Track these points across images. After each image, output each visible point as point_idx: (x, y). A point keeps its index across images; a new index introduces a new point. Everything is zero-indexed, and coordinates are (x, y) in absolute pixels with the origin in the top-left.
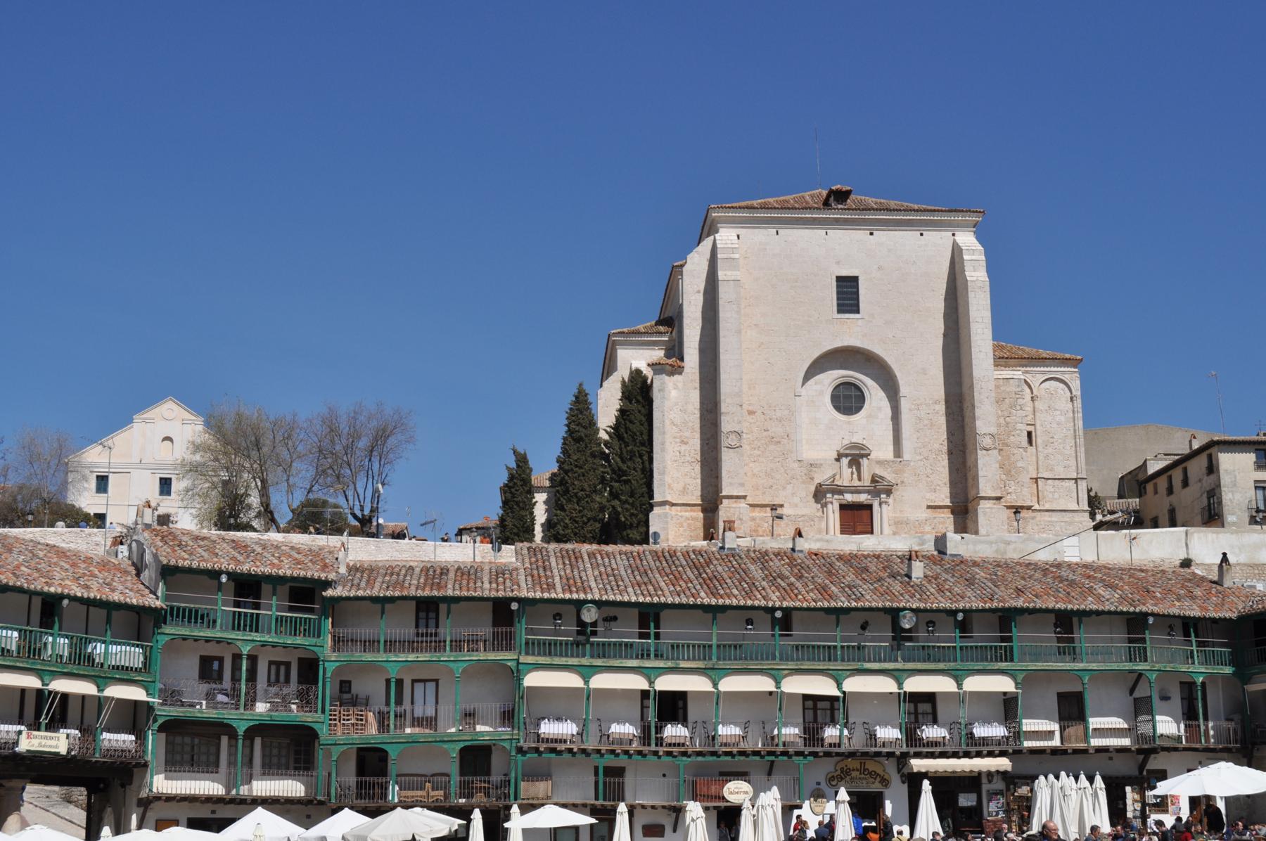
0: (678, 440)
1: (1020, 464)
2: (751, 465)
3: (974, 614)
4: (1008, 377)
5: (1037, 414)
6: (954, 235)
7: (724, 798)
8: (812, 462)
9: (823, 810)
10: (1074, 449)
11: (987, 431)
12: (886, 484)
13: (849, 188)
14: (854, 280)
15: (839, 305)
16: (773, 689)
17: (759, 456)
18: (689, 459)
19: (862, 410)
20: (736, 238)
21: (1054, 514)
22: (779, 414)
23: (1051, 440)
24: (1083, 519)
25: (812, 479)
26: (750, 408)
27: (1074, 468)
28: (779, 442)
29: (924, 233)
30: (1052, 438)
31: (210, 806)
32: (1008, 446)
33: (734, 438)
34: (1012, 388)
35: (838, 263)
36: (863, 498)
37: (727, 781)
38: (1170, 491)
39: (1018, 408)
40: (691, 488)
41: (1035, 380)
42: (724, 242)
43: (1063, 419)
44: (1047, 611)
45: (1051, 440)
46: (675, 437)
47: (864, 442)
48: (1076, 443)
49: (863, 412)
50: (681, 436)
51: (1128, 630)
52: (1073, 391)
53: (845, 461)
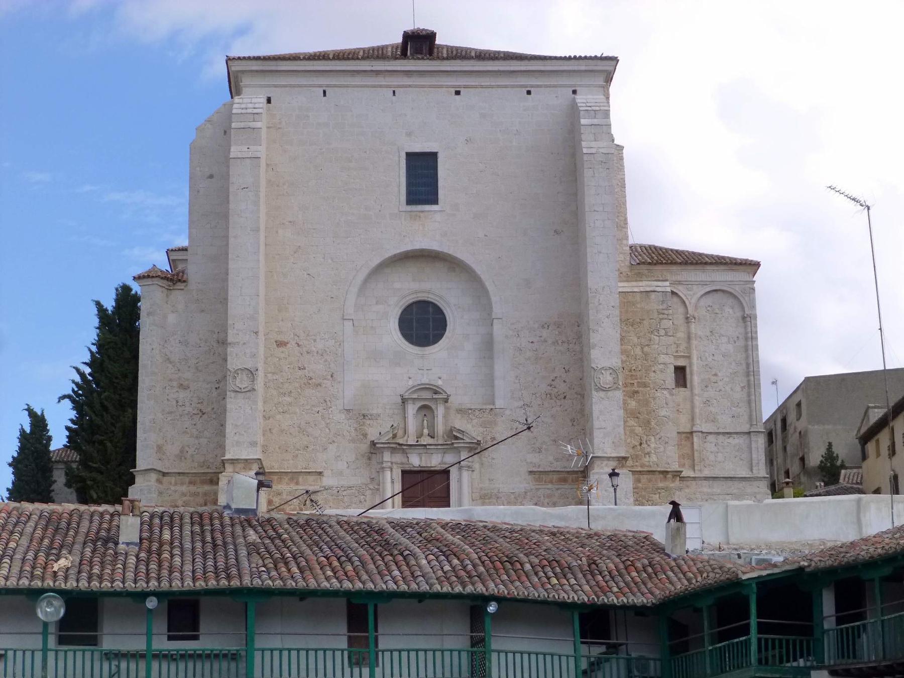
0: (175, 384)
1: (663, 412)
2: (279, 417)
3: (107, 600)
4: (648, 289)
5: (694, 342)
6: (574, 92)
10: (746, 390)
11: (607, 364)
12: (468, 440)
14: (432, 157)
15: (409, 193)
17: (290, 404)
18: (191, 410)
20: (265, 101)
21: (716, 484)
22: (320, 345)
23: (714, 379)
24: (757, 490)
26: (280, 338)
27: (746, 417)
29: (532, 90)
30: (716, 375)
32: (645, 385)
33: (245, 378)
34: (654, 304)
35: (409, 134)
36: (435, 461)
39: (662, 332)
40: (191, 451)
41: (692, 295)
42: (243, 106)
43: (730, 347)
44: (335, 594)
45: (714, 379)
46: (171, 380)
47: (440, 383)
48: (749, 381)
49: (443, 342)
50: (179, 378)
51: (472, 627)
52: (746, 309)
53: (411, 409)
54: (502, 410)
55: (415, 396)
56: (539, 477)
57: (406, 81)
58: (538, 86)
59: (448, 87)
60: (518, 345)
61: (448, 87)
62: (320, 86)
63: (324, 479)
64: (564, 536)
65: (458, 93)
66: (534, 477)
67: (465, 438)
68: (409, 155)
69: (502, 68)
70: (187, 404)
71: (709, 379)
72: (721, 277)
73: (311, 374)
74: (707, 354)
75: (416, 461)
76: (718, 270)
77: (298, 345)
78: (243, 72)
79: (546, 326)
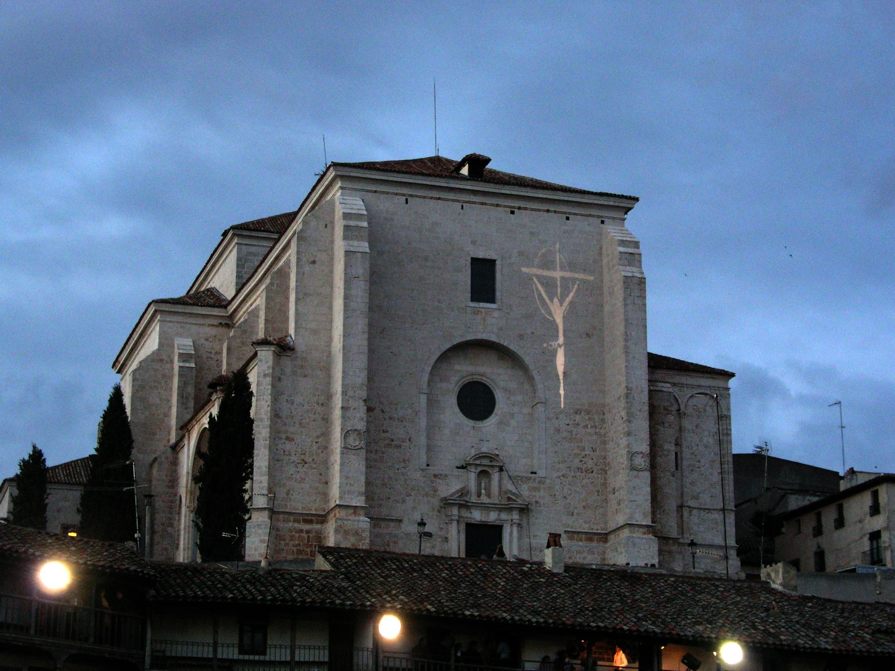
14: (491, 263)
17: (376, 461)
29: (570, 216)
35: (474, 243)
36: (492, 517)
45: (697, 464)
54: (543, 479)
55: (478, 462)
56: (572, 536)
57: (522, 204)
58: (575, 214)
59: (505, 206)
60: (557, 425)
61: (505, 206)
63: (403, 526)
64: (302, 598)
65: (512, 213)
66: (568, 536)
67: (518, 500)
68: (473, 259)
70: (293, 454)
71: (694, 465)
72: (705, 382)
73: (393, 437)
74: (693, 444)
75: (477, 516)
76: (708, 378)
77: (383, 412)
79: (579, 412)
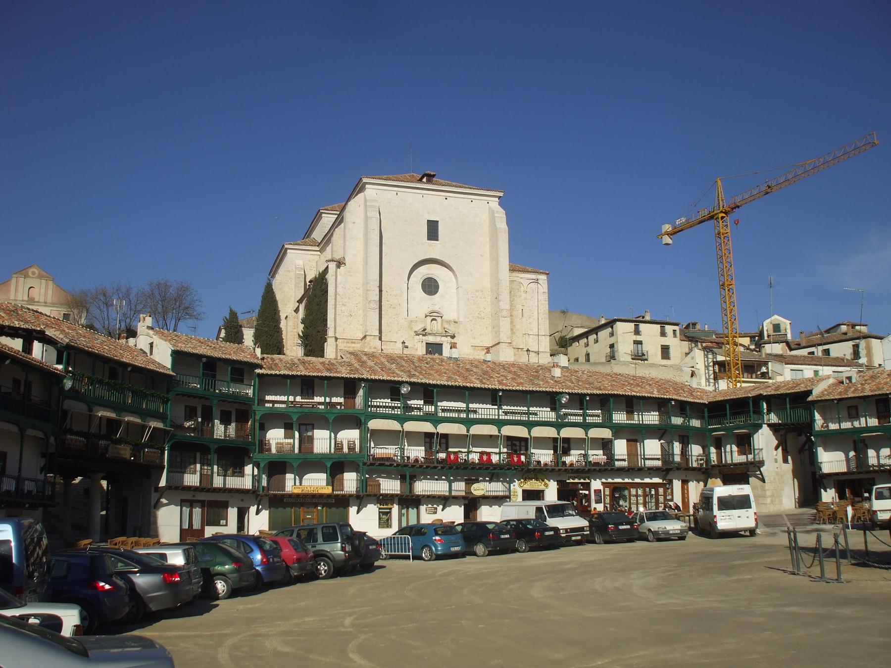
7: (471, 492)
8: (412, 320)
9: (516, 500)
13: (434, 173)
16: (496, 433)
19: (438, 293)
25: (412, 328)
28: (395, 308)
31: (192, 493)
37: (473, 484)
38: (587, 345)
45: (532, 315)
51: (601, 405)
62: (396, 191)
63: (856, 439)
65: (446, 199)
69: (463, 191)
78: (367, 183)
